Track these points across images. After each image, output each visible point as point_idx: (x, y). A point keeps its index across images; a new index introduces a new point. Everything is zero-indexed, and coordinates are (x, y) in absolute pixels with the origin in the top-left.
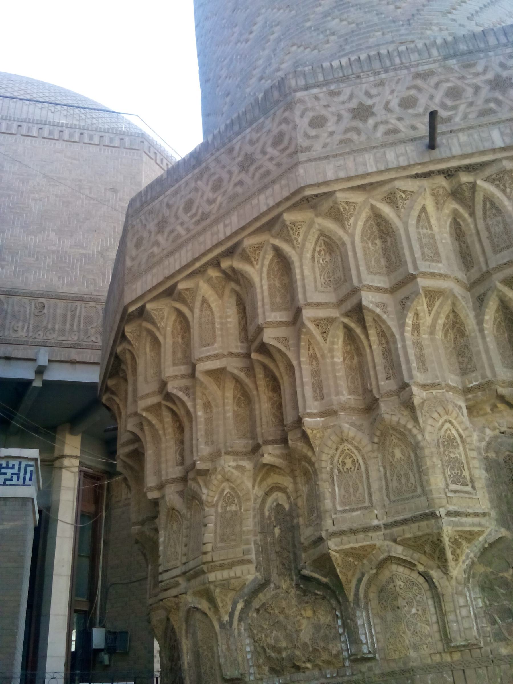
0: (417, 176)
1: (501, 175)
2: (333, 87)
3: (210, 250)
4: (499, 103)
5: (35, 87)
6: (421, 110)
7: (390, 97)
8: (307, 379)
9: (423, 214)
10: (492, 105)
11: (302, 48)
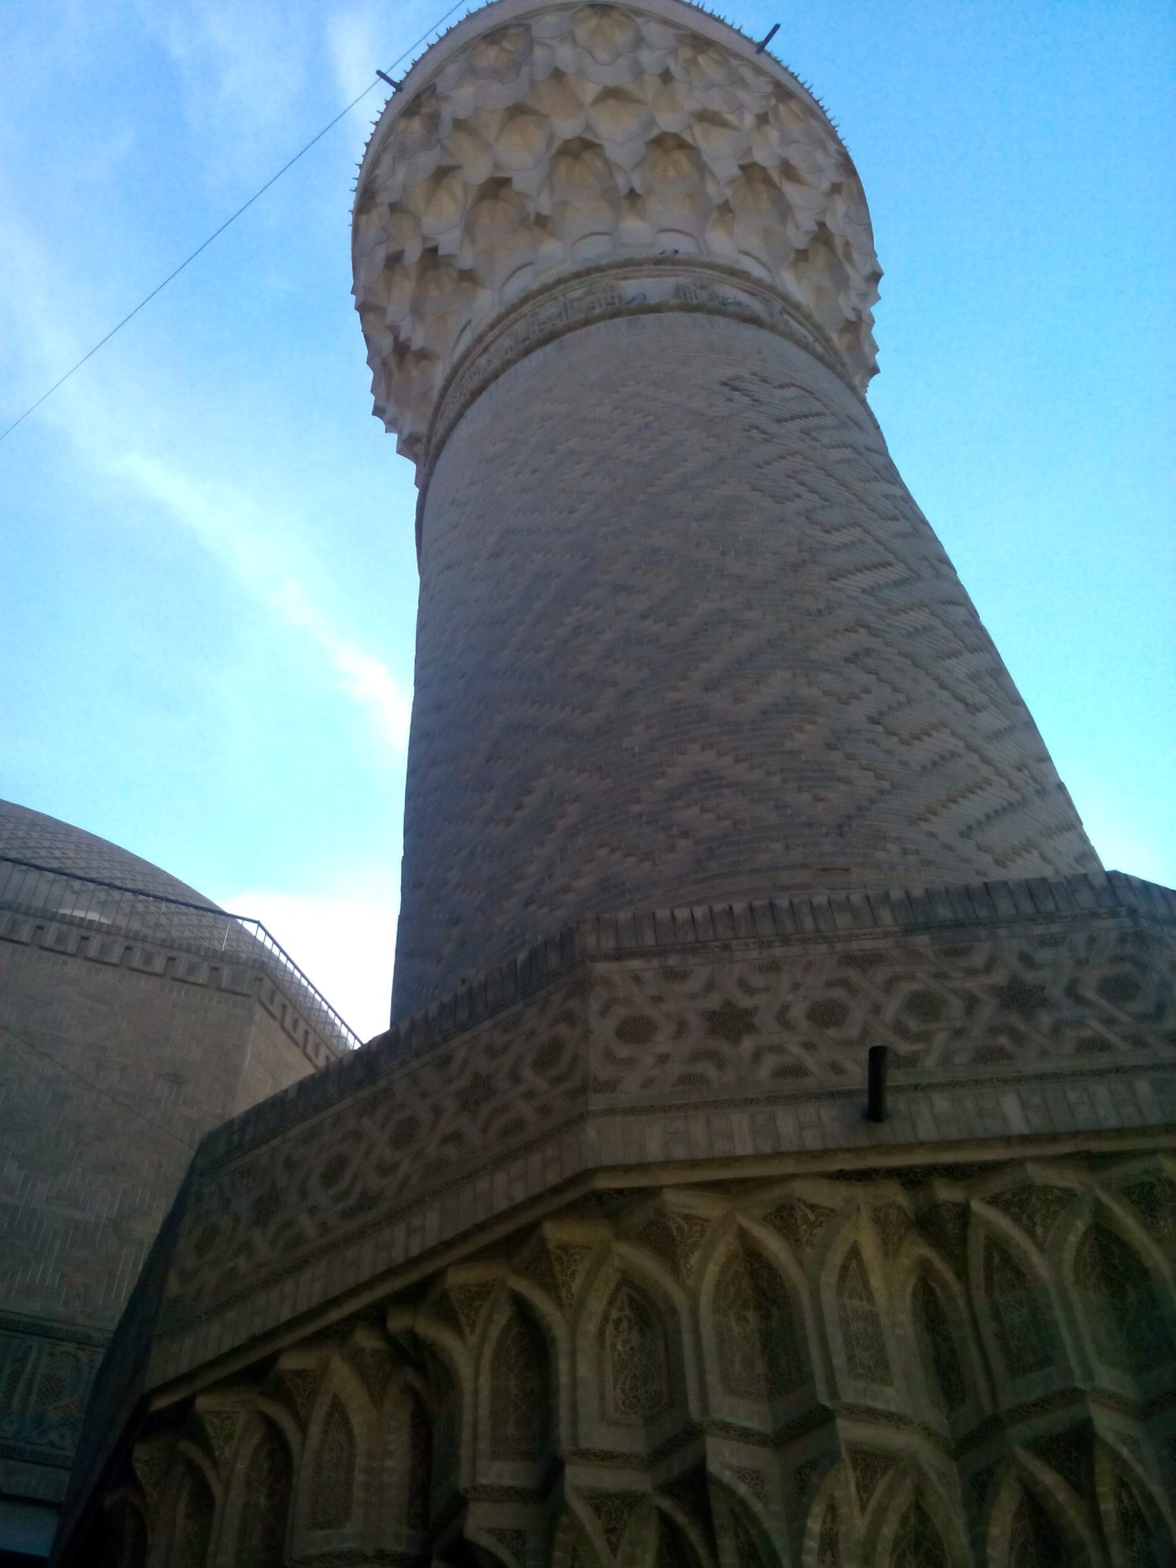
0: (841, 1176)
1: (1025, 1196)
2: (672, 961)
3: (368, 1285)
4: (1018, 1038)
5: (48, 836)
6: (853, 1032)
7: (789, 998)
9: (854, 1264)
10: (1003, 1041)
11: (619, 855)
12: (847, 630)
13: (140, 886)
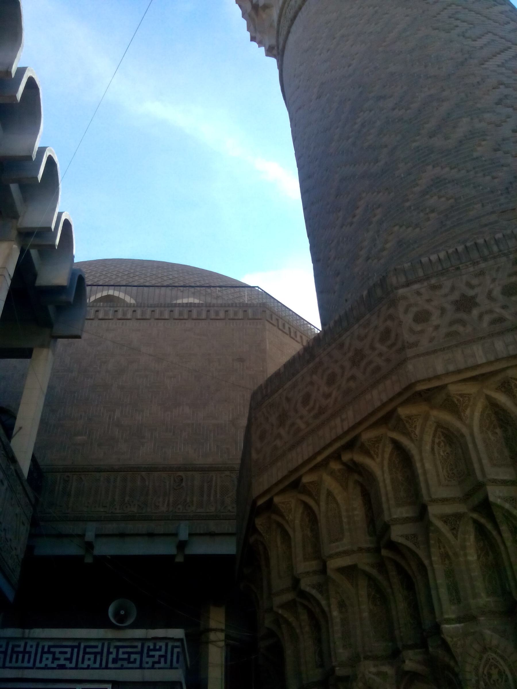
2: (433, 281)
3: (330, 445)
5: (165, 271)
7: (492, 286)
8: (441, 580)
11: (404, 227)
12: (494, 88)
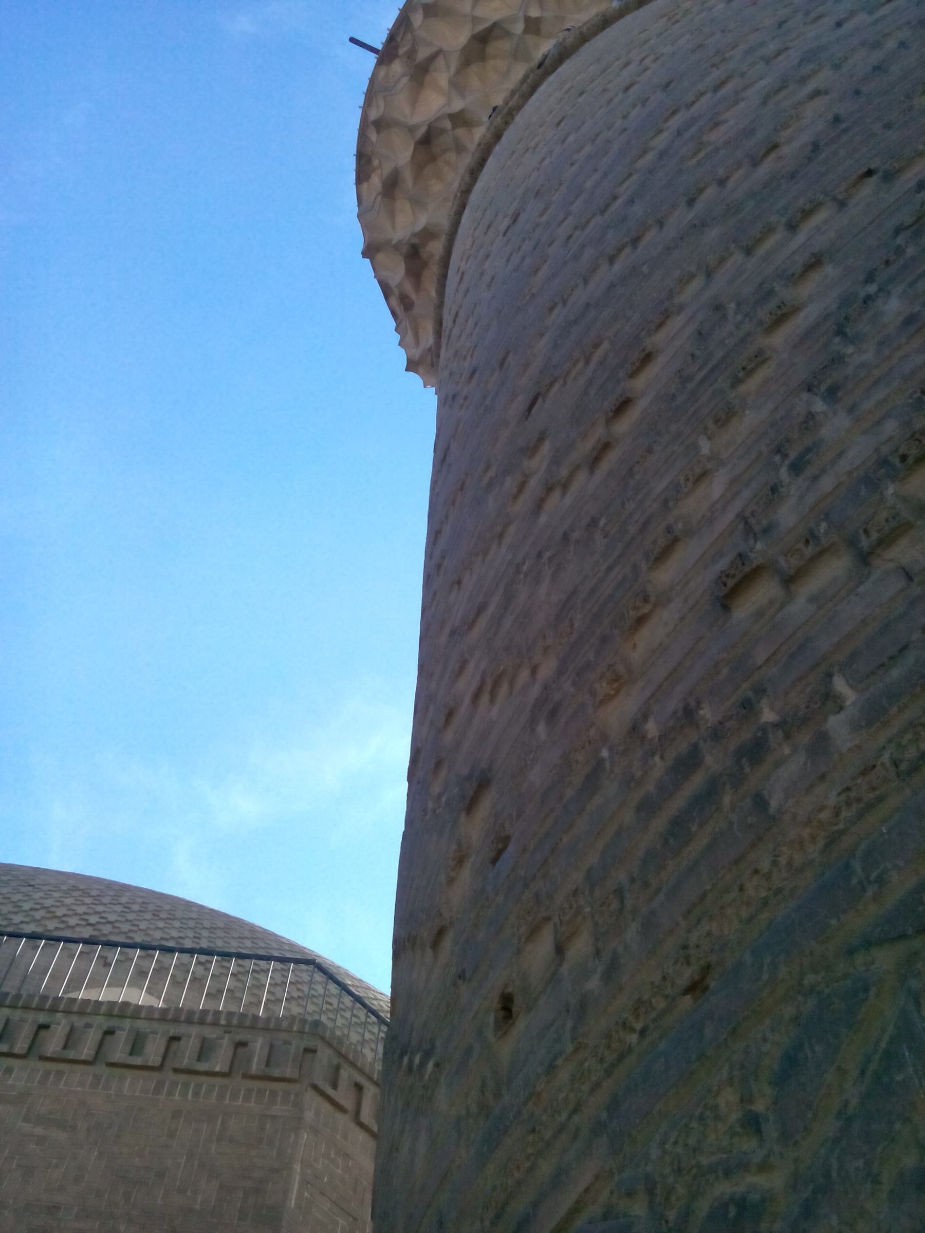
13: (204, 944)
